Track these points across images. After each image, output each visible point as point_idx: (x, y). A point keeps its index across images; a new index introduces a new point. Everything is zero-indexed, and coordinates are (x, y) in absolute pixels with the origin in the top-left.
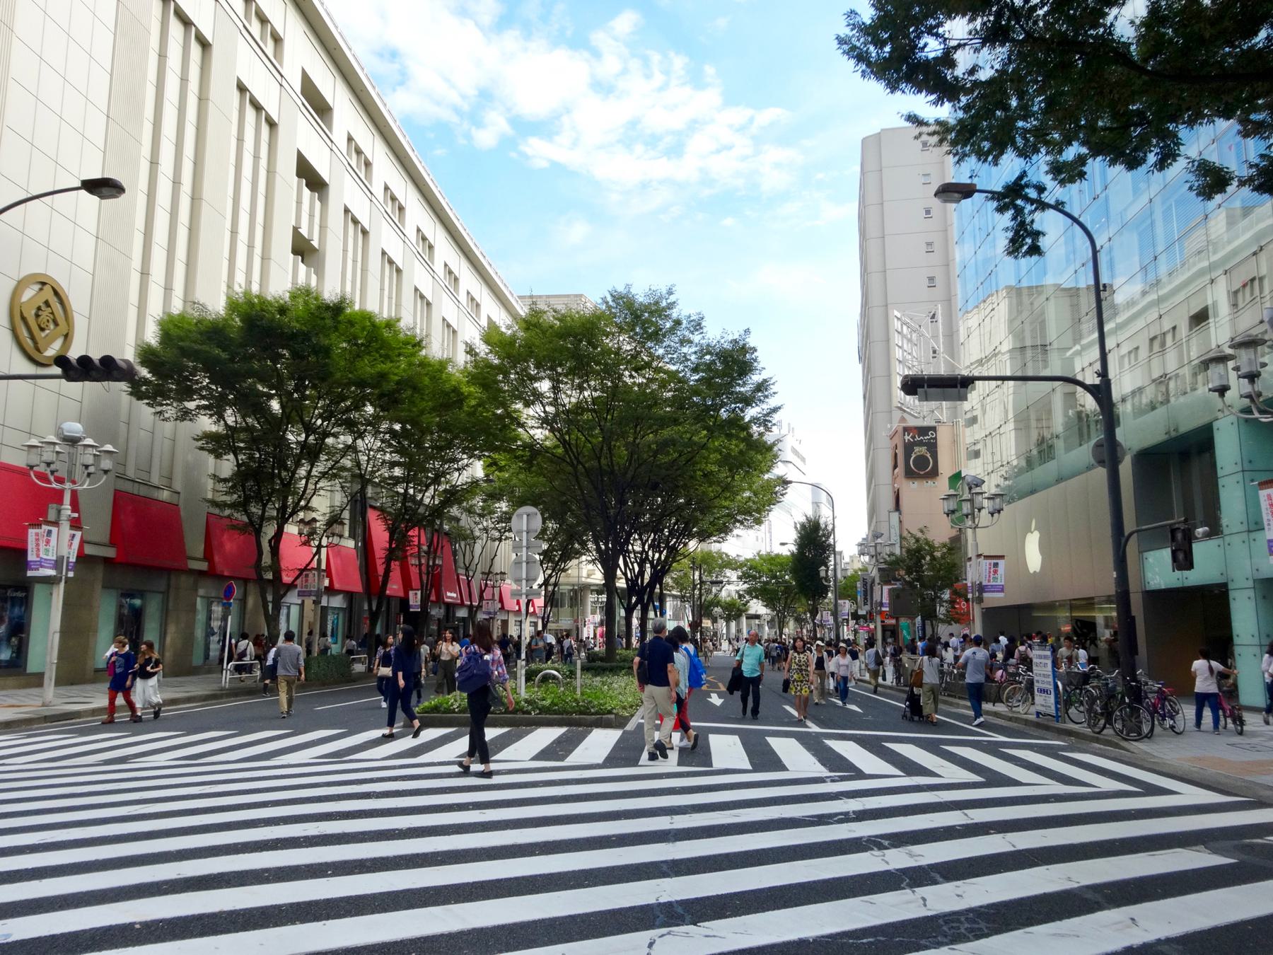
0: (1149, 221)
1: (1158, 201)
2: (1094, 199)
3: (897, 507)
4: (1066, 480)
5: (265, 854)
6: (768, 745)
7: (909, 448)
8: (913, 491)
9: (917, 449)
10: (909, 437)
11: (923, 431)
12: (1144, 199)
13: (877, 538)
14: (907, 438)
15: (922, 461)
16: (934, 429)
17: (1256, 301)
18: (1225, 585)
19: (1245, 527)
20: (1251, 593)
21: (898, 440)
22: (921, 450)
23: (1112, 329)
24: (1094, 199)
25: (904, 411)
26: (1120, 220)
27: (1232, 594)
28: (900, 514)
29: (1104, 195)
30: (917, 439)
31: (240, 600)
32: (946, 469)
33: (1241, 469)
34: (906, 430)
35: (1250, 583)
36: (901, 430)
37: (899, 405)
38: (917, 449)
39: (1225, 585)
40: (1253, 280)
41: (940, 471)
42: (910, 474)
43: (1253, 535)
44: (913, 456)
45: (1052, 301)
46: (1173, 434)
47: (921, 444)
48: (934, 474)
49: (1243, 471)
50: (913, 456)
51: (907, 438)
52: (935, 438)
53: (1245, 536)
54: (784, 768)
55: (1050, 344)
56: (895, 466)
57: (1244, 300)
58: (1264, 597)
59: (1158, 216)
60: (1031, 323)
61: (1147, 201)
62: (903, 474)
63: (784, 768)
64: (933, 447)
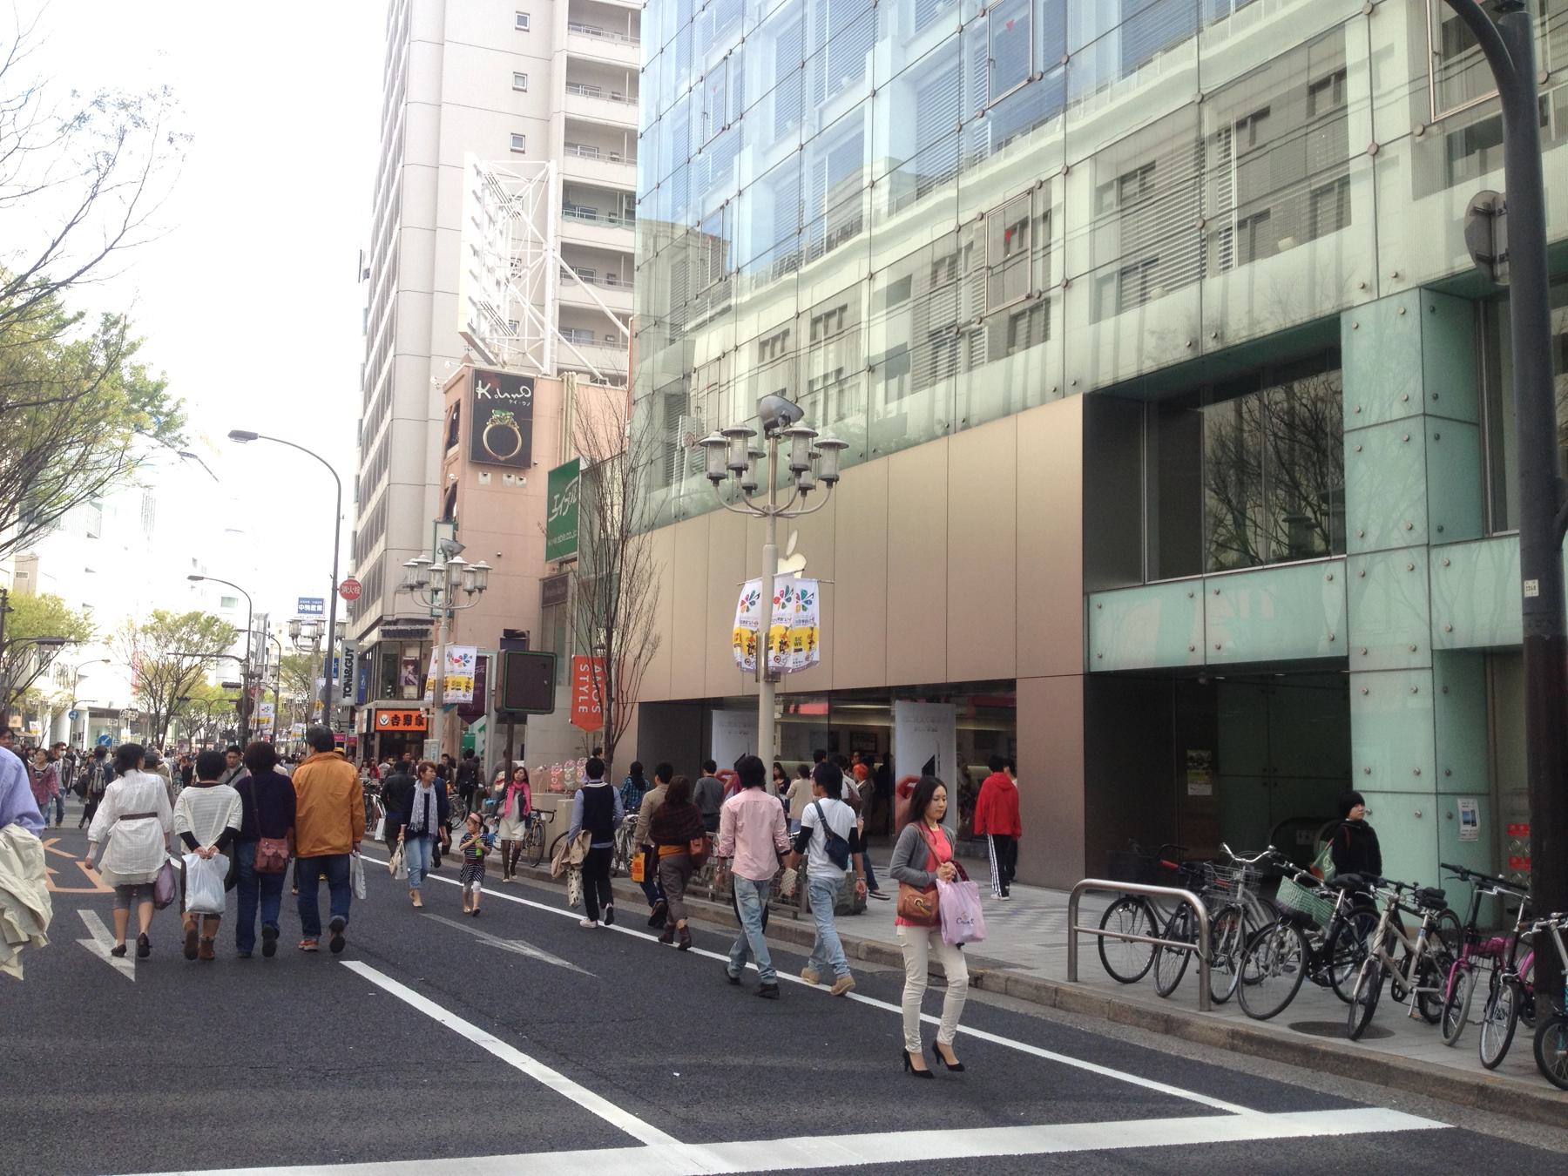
0: (955, 62)
1: (809, 148)
2: (724, 129)
3: (448, 516)
4: (887, 453)
5: (1087, 253)
6: (136, 979)
7: (482, 410)
8: (479, 486)
9: (496, 415)
10: (484, 391)
11: (512, 383)
12: (792, 145)
13: (453, 554)
14: (480, 391)
15: (502, 438)
16: (530, 382)
17: (1024, 255)
18: (1343, 662)
19: (1419, 534)
20: (1424, 680)
21: (460, 393)
22: (507, 417)
23: (950, 199)
24: (724, 129)
25: (474, 345)
26: (817, 122)
27: (1356, 684)
28: (456, 528)
29: (738, 125)
30: (499, 395)
31: (1488, 795)
32: (545, 456)
33: (1422, 411)
34: (480, 376)
35: (1423, 658)
36: (469, 374)
37: (469, 332)
38: (496, 415)
39: (1343, 662)
40: (1024, 224)
41: (534, 459)
42: (479, 459)
43: (1440, 555)
44: (489, 426)
45: (884, 101)
46: (1210, 346)
47: (504, 405)
48: (522, 463)
49: (1425, 415)
50: (489, 426)
51: (480, 391)
52: (531, 399)
53: (1418, 557)
54: (95, 887)
55: (738, 270)
56: (451, 443)
57: (966, 270)
58: (1446, 691)
59: (807, 169)
60: (816, 153)
61: (797, 146)
62: (468, 453)
63: (95, 887)
64: (524, 413)
